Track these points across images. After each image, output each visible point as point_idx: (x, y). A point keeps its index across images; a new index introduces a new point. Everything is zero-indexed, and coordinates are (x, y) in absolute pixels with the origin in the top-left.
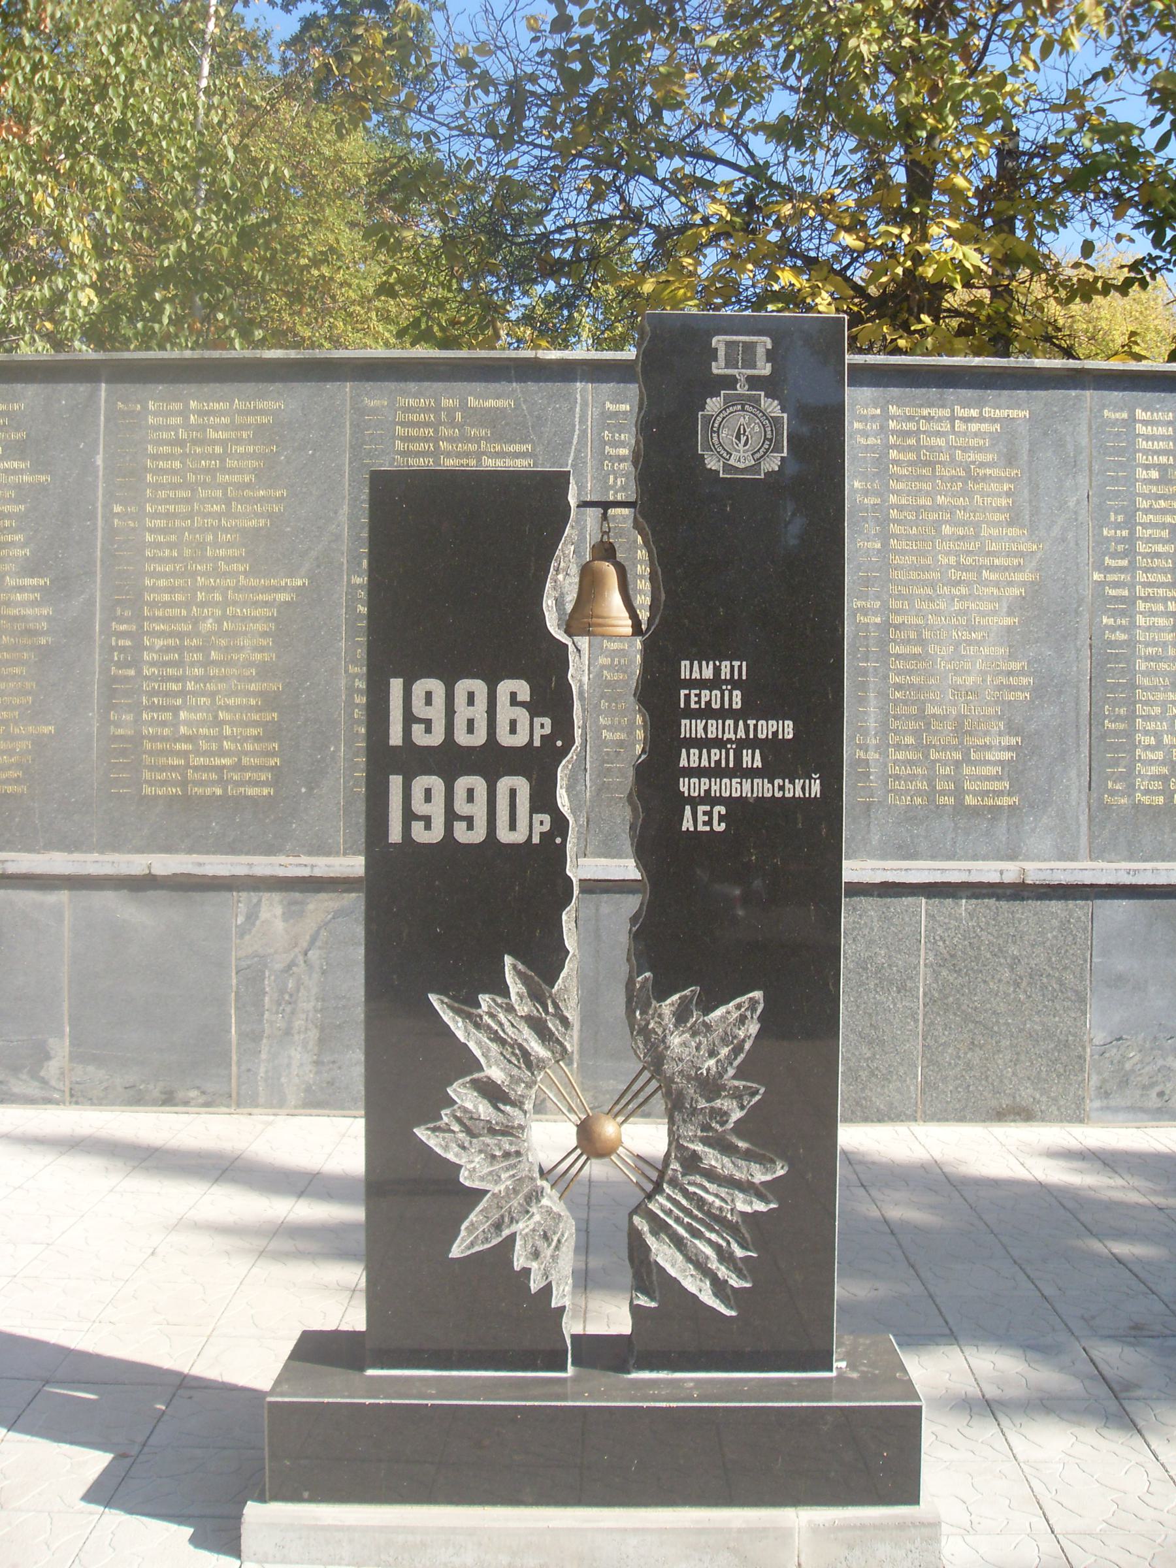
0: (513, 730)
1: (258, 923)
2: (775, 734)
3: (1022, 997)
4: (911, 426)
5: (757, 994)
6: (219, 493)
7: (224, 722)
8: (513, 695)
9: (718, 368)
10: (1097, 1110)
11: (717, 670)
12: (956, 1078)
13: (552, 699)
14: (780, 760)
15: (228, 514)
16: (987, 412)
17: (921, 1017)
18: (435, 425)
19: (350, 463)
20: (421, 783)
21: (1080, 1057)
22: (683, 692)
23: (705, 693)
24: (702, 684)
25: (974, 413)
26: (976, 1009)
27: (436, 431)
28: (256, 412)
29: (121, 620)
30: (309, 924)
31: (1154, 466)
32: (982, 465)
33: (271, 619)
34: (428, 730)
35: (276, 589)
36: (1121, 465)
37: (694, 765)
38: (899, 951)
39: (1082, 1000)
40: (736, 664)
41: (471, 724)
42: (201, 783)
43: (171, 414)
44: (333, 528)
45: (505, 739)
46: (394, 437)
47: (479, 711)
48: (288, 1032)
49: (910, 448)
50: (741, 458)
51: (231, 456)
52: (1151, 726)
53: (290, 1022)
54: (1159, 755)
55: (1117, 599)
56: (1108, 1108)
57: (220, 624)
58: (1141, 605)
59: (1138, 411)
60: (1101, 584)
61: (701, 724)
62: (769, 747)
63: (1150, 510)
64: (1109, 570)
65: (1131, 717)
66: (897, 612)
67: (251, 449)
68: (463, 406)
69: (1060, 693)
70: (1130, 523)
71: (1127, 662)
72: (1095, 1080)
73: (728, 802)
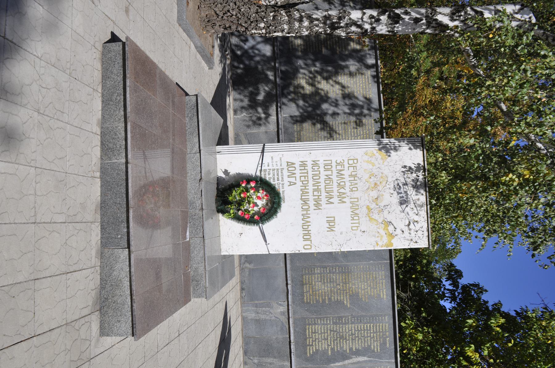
29: (339, 269)
30: (280, 317)
43: (382, 276)
44: (360, 312)
48: (258, 313)
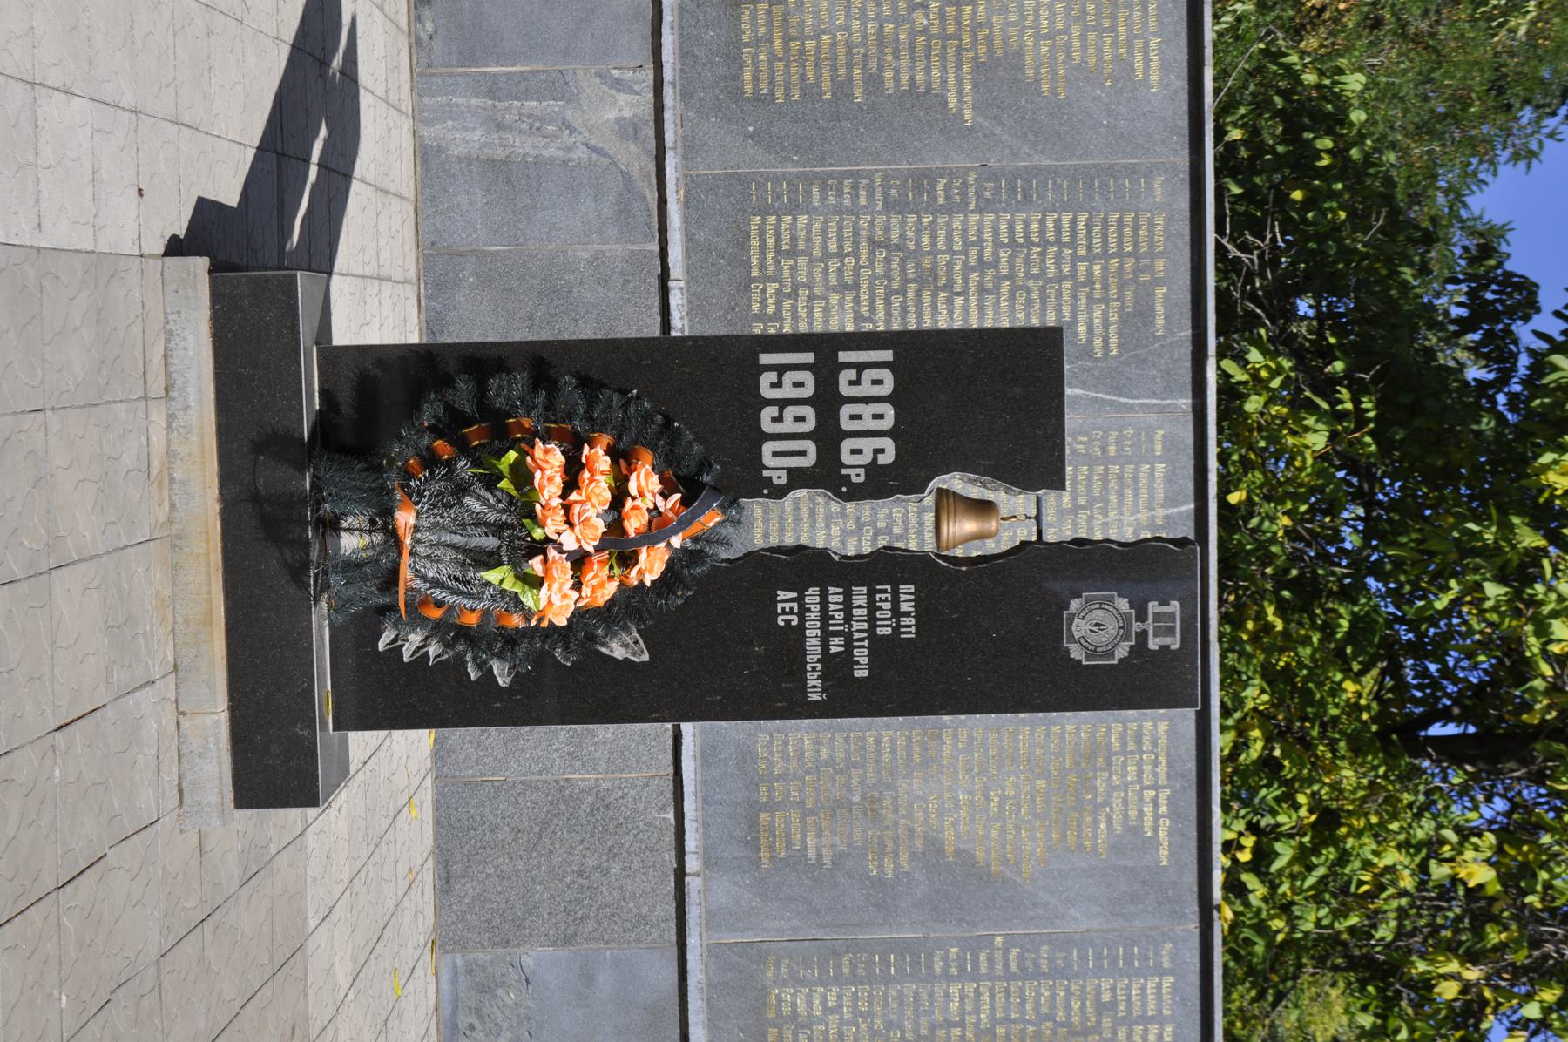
0: (854, 452)
1: (613, 92)
2: (858, 663)
3: (568, 880)
4: (1147, 746)
5: (646, 657)
6: (1060, 26)
7: (819, 40)
8: (882, 451)
9: (1153, 607)
10: (454, 963)
11: (907, 614)
12: (482, 816)
13: (880, 483)
14: (836, 667)
15: (1038, 36)
16: (1165, 824)
17: (544, 777)
18: (1134, 254)
19: (1095, 166)
20: (808, 378)
21: (508, 941)
22: (889, 588)
23: (889, 605)
24: (896, 602)
25: (1163, 809)
26: (554, 833)
27: (1129, 254)
28: (1147, 62)
30: (614, 147)
31: (1114, 996)
32: (1109, 819)
33: (929, 89)
34: (852, 383)
35: (960, 93)
36: (1114, 962)
37: (830, 598)
38: (611, 753)
39: (568, 940)
40: (913, 629)
41: (859, 417)
42: (754, 18)
45: (847, 445)
46: (1122, 210)
47: (869, 424)
48: (500, 127)
49: (1124, 744)
50: (1080, 628)
51: (1100, 37)
52: (847, 1002)
53: (511, 128)
54: (818, 1011)
55: (976, 963)
56: (456, 974)
57: (921, 33)
58: (970, 987)
59: (1171, 979)
60: (991, 945)
61: (863, 603)
62: (847, 658)
63: (1069, 993)
64: (1006, 952)
65: (855, 980)
66: (955, 736)
67: (1107, 56)
68: (1157, 282)
69: (877, 905)
70: (1058, 973)
71: (912, 975)
72: (483, 957)
73: (801, 627)
